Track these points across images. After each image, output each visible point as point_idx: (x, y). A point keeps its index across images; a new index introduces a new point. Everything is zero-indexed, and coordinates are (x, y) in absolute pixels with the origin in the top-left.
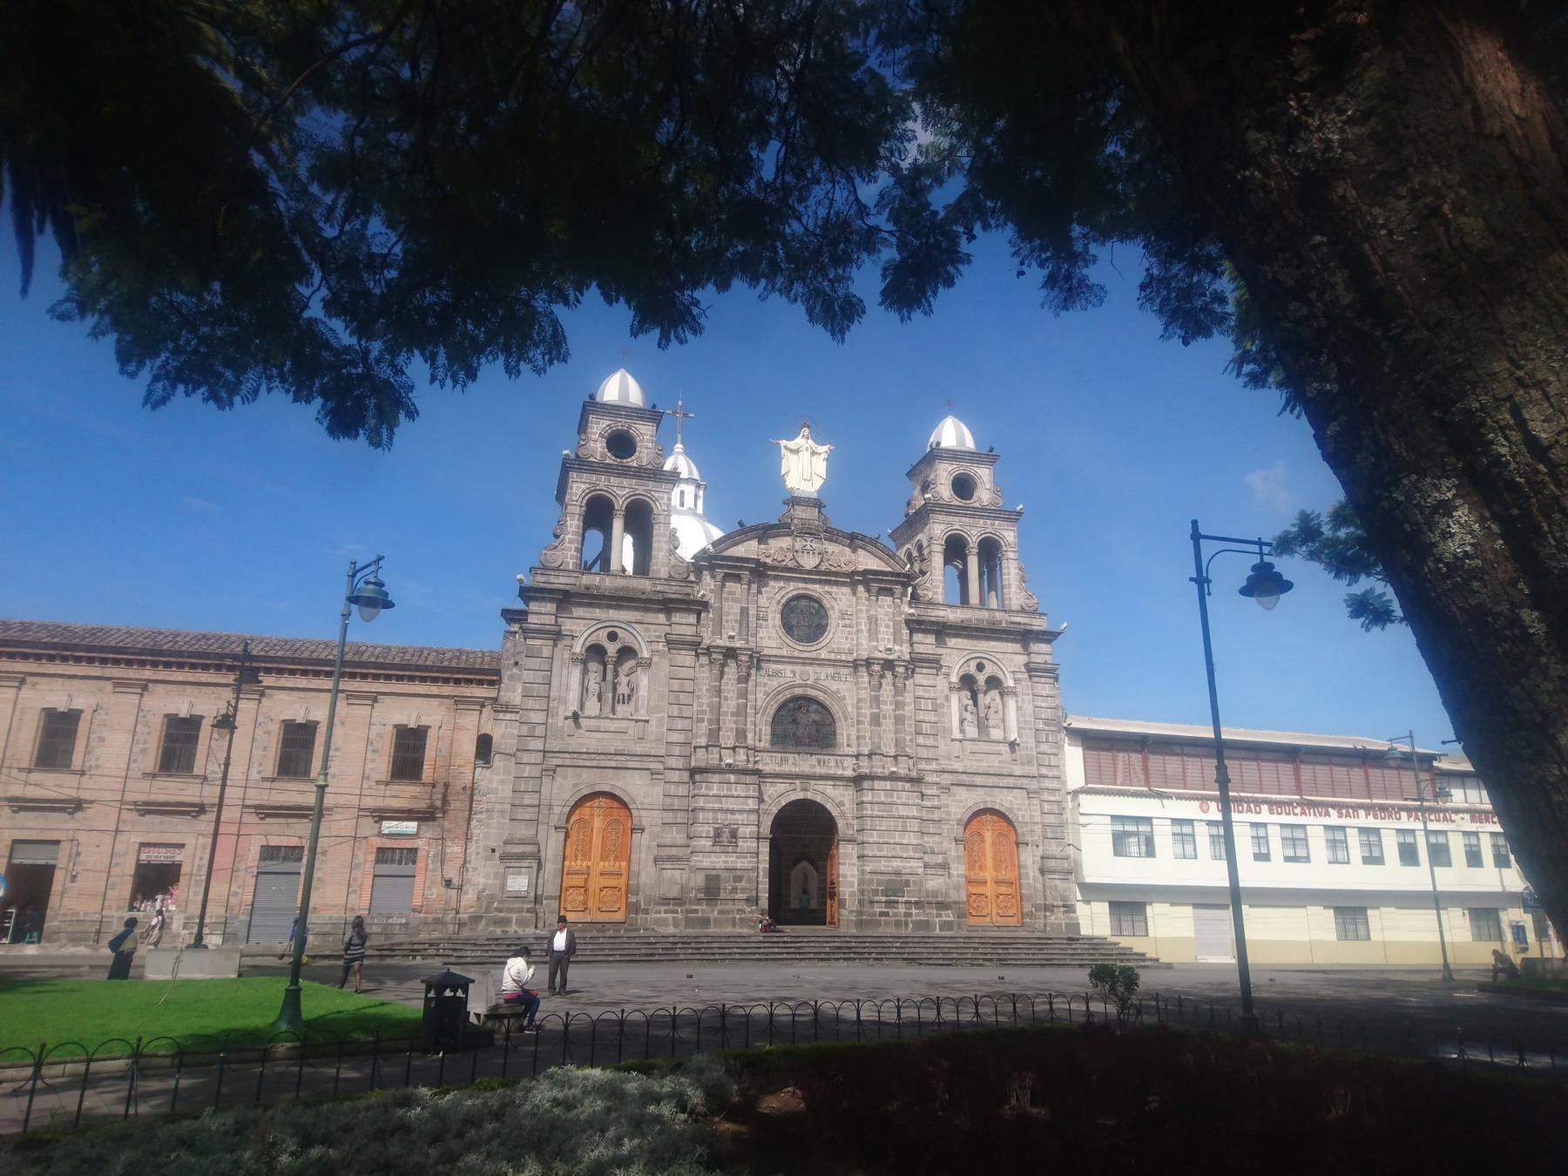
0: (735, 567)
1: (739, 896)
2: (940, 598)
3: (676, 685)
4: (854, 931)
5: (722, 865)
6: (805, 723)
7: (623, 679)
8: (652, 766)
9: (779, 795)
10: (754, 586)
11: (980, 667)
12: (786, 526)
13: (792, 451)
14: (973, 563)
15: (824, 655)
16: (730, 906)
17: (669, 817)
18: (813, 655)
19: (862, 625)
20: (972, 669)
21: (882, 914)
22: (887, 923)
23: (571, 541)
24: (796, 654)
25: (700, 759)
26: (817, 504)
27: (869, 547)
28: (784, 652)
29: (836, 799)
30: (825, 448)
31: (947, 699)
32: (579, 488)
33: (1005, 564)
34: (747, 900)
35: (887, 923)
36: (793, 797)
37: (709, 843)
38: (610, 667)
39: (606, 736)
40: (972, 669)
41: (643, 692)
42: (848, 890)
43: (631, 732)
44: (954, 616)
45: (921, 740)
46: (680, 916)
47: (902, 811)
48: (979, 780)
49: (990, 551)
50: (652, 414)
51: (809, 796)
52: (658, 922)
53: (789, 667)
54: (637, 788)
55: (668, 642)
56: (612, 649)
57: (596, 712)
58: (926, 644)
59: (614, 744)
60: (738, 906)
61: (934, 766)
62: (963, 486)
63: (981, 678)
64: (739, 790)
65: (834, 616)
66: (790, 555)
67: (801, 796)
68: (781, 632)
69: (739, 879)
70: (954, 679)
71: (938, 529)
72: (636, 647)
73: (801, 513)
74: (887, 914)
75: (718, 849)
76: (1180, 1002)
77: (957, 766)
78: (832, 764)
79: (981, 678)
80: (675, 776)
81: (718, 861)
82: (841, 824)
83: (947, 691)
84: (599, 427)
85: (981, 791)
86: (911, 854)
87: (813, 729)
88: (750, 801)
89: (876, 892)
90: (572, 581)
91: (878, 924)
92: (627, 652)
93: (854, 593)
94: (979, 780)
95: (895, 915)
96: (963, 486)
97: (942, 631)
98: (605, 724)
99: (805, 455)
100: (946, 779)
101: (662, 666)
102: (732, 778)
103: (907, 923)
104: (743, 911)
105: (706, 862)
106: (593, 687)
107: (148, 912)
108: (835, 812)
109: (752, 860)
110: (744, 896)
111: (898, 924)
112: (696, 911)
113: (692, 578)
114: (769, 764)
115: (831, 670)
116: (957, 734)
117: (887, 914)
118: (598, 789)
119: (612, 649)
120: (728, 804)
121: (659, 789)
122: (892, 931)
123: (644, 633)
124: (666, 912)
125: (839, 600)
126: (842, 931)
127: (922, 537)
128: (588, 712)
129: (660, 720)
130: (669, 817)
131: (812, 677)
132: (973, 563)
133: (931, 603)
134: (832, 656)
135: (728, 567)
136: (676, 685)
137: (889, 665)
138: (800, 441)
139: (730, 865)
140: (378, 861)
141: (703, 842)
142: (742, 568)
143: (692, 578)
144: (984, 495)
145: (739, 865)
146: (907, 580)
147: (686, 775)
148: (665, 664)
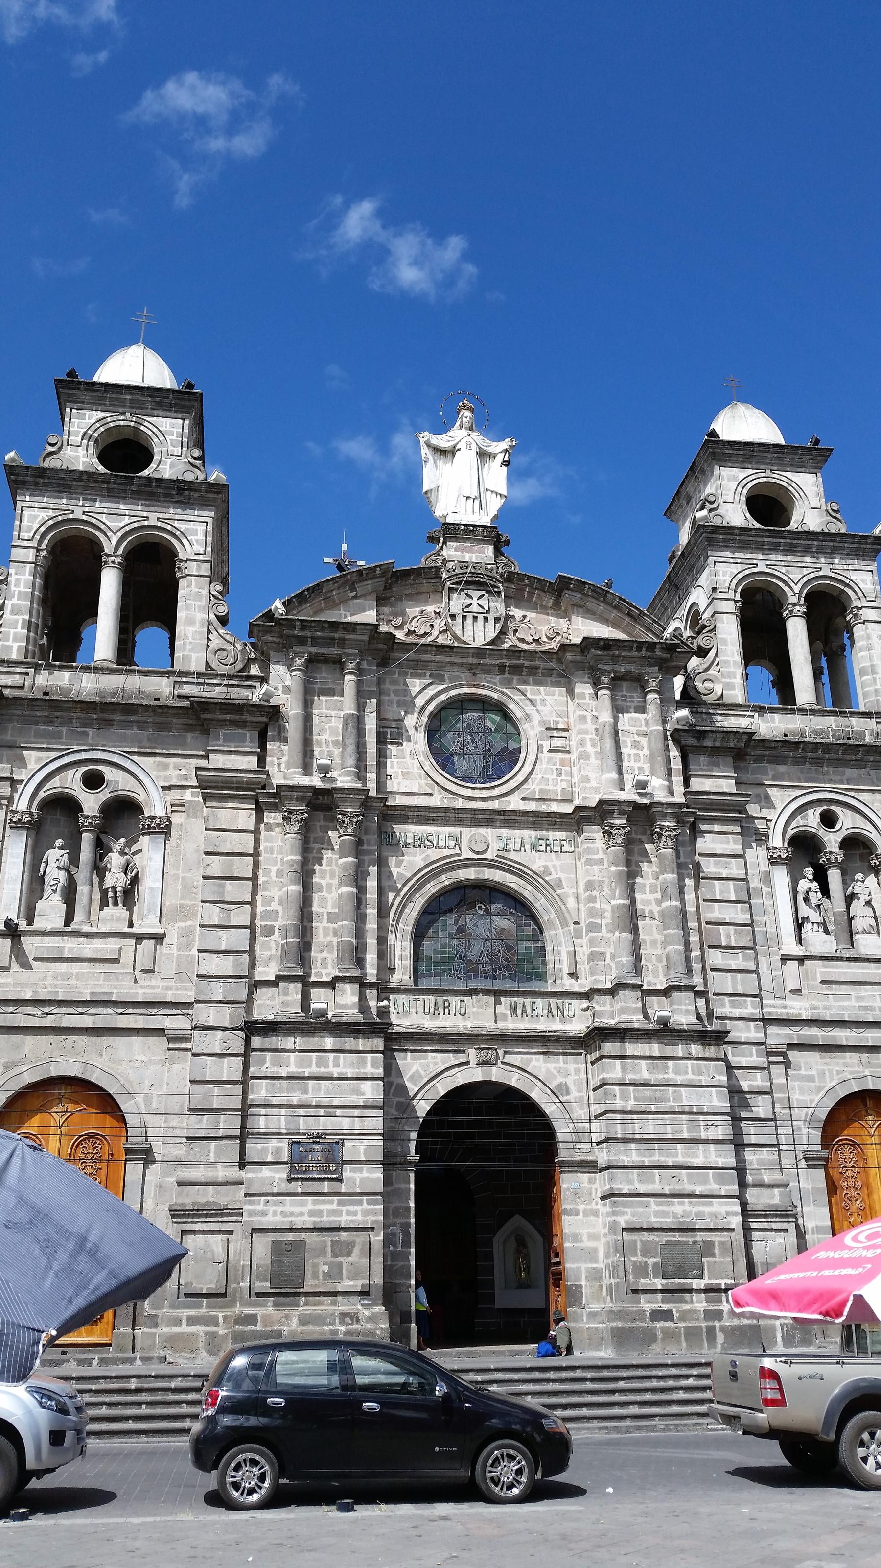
0: (331, 642)
1: (347, 1284)
2: (737, 695)
3: (217, 865)
4: (605, 1354)
5: (308, 1221)
6: (481, 928)
7: (115, 860)
8: (167, 1023)
9: (429, 1077)
10: (370, 678)
11: (828, 820)
12: (434, 573)
13: (440, 452)
14: (797, 633)
15: (515, 803)
16: (325, 1307)
17: (203, 1124)
18: (495, 805)
19: (581, 744)
20: (812, 821)
21: (657, 1315)
22: (670, 1336)
23: (16, 611)
24: (460, 803)
25: (271, 1005)
26: (492, 535)
27: (591, 604)
28: (435, 801)
29: (556, 1084)
30: (504, 445)
31: (767, 879)
32: (35, 516)
33: (859, 631)
34: (364, 1293)
35: (670, 1336)
36: (461, 1078)
37: (282, 1173)
38: (87, 839)
39: (75, 967)
40: (812, 821)
41: (150, 884)
42: (584, 1266)
43: (127, 957)
44: (772, 726)
45: (716, 958)
46: (221, 1331)
47: (689, 1098)
48: (843, 1036)
49: (829, 613)
50: (182, 401)
51: (496, 1074)
52: (174, 1342)
53: (445, 831)
54: (144, 1076)
55: (203, 784)
56: (91, 803)
57: (58, 923)
58: (719, 782)
59: (87, 983)
60: (344, 1305)
61: (749, 1008)
62: (769, 506)
63: (832, 841)
64: (345, 1065)
65: (531, 733)
66: (439, 624)
67: (476, 1074)
68: (429, 764)
69: (346, 1250)
70: (777, 841)
71: (723, 573)
72: (141, 798)
73: (454, 553)
74: (667, 1315)
75: (299, 1187)
76: (555, 1199)
77: (799, 1008)
78: (541, 1011)
79: (832, 841)
80: (215, 1042)
81: (302, 1211)
82: (563, 1131)
83: (764, 866)
84: (84, 422)
85: (851, 1058)
86: (713, 1187)
87: (500, 947)
88: (366, 1086)
89: (642, 1270)
90: (17, 680)
91: (648, 1338)
92: (123, 813)
93: (571, 692)
94: (843, 1036)
95: (684, 1316)
96: (769, 506)
97: (743, 751)
98: (70, 946)
99: (466, 458)
100: (778, 1036)
101: (191, 832)
102: (329, 1042)
103: (711, 1331)
104: (355, 1318)
105: (274, 1214)
106: (54, 875)
107: (155, 1361)
108: (550, 1109)
109: (359, 1206)
110: (357, 1285)
111: (692, 1334)
112: (251, 1319)
113: (254, 670)
114: (407, 1014)
115: (530, 835)
116: (790, 947)
117: (667, 1315)
118: (54, 1072)
119: (91, 803)
120: (320, 1092)
121: (183, 1067)
122: (682, 1352)
123: (154, 778)
124: (192, 1321)
125: (538, 707)
126: (579, 1356)
127: (698, 596)
128: (39, 923)
129: (186, 934)
130: (203, 1124)
131: (494, 846)
132: (797, 633)
133: (721, 705)
134: (532, 806)
135: (315, 641)
136: (217, 865)
137: (642, 817)
138: (458, 435)
139: (326, 1221)
140: (862, 1350)
141: (266, 1172)
142: (342, 643)
143: (254, 670)
144: (810, 511)
145: (344, 1220)
146: (671, 657)
147: (236, 1042)
148: (197, 826)
